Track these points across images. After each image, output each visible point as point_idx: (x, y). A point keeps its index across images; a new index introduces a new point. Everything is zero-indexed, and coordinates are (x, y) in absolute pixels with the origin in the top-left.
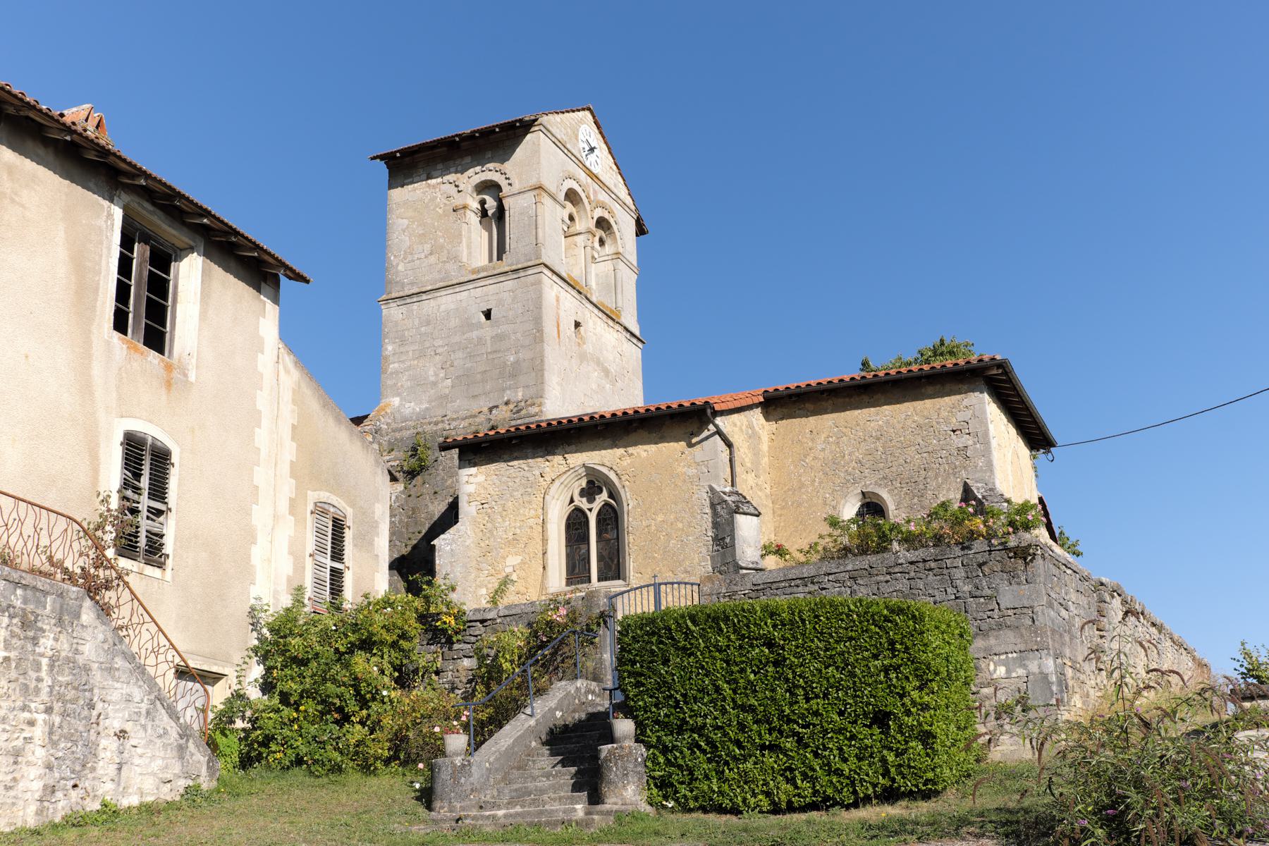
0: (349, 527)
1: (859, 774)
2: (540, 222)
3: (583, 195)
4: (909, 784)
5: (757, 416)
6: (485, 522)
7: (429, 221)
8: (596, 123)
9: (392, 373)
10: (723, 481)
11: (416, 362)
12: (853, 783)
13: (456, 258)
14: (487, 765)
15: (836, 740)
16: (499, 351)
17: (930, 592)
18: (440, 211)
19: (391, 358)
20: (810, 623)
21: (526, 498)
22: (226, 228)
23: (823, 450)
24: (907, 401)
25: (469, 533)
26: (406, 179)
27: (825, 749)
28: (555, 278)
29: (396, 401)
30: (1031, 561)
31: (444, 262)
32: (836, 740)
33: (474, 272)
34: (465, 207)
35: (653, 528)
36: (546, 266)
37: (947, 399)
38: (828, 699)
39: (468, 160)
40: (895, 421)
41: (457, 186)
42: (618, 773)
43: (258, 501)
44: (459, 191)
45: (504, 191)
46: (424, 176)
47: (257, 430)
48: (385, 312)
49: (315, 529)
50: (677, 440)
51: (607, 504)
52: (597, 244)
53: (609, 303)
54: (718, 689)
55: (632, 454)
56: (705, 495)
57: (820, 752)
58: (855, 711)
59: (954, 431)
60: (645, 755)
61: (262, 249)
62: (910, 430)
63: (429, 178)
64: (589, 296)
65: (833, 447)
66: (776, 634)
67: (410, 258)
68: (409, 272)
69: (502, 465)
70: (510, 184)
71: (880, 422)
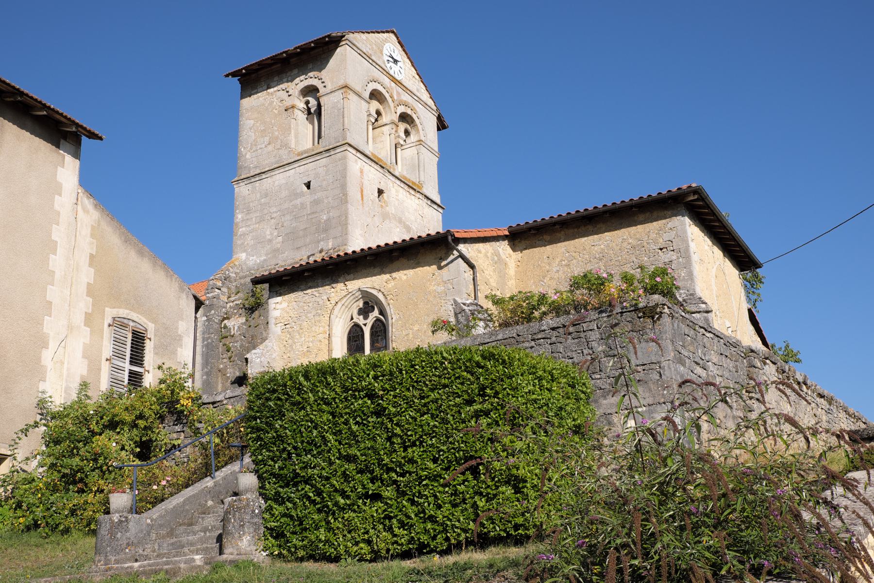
0: (150, 339)
1: (451, 520)
2: (346, 112)
3: (387, 96)
4: (498, 529)
5: (504, 247)
6: (287, 339)
7: (268, 120)
8: (399, 42)
9: (241, 235)
10: (465, 296)
11: (257, 225)
12: (445, 531)
13: (286, 146)
14: (149, 521)
15: (431, 487)
16: (316, 212)
17: (569, 354)
18: (276, 112)
19: (240, 224)
20: (407, 373)
21: (317, 318)
22: (11, 89)
23: (558, 271)
24: (624, 228)
25: (275, 348)
26: (252, 90)
27: (421, 496)
28: (359, 155)
29: (243, 256)
30: (658, 319)
31: (279, 149)
32: (431, 487)
33: (299, 155)
34: (293, 107)
35: (411, 336)
36: (350, 145)
37: (655, 223)
38: (423, 447)
39: (295, 71)
40: (614, 244)
41: (288, 92)
42: (236, 524)
43: (51, 314)
44: (289, 96)
45: (320, 92)
46: (265, 87)
47: (52, 256)
48: (236, 190)
49: (113, 339)
50: (430, 265)
51: (378, 320)
52: (402, 135)
53: (413, 178)
54: (325, 440)
55: (395, 278)
56: (451, 308)
57: (416, 499)
58: (447, 457)
59: (661, 249)
60: (263, 507)
61: (49, 107)
62: (626, 250)
63: (269, 88)
64: (391, 171)
65: (566, 268)
66: (376, 385)
67: (254, 149)
68: (253, 159)
69: (300, 293)
70: (325, 87)
71: (602, 246)
